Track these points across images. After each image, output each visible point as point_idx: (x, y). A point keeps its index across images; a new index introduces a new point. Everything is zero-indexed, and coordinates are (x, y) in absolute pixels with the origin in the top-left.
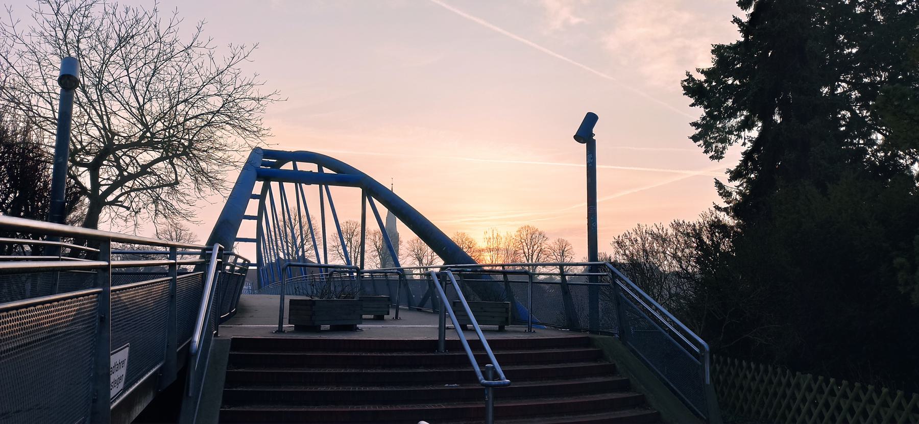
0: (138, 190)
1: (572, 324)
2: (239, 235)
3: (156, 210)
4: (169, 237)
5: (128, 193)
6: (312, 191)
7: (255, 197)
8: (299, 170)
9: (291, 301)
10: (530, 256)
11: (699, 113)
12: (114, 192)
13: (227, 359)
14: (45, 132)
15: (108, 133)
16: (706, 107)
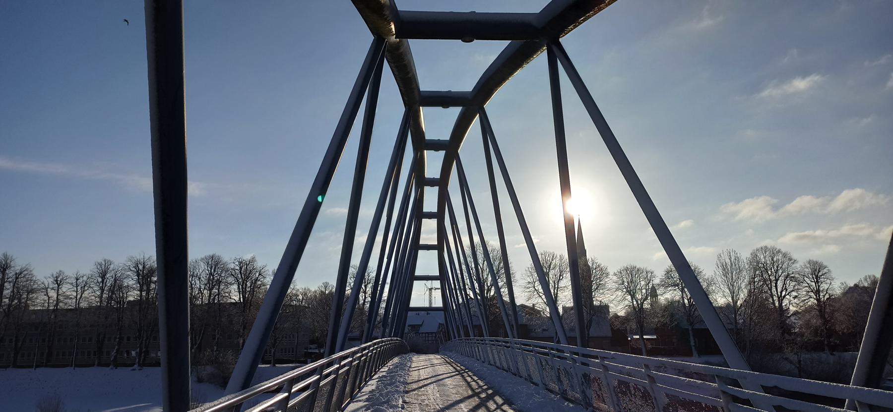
2: (418, 273)
7: (430, 216)
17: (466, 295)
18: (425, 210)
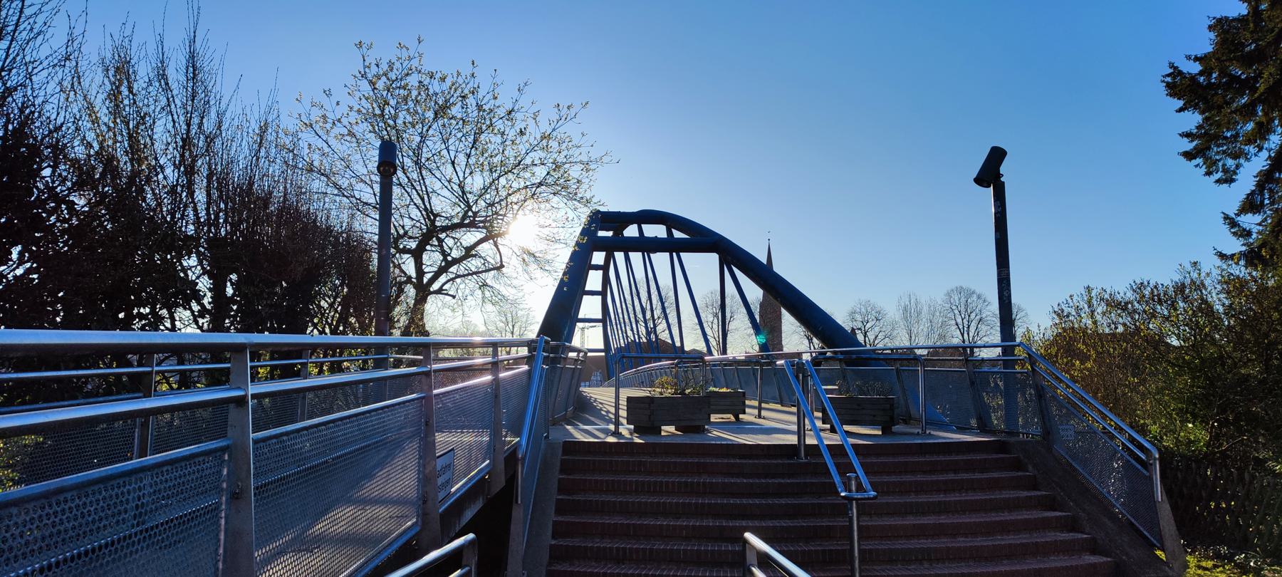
0: (464, 276)
1: (984, 428)
2: (581, 316)
3: (483, 298)
4: (504, 320)
5: (452, 279)
6: (661, 260)
7: (597, 267)
8: (623, 253)
9: (629, 399)
10: (966, 329)
11: (1193, 120)
12: (440, 279)
13: (559, 464)
14: (368, 219)
15: (431, 215)
16: (1202, 113)
17: (627, 337)
18: (600, 297)
